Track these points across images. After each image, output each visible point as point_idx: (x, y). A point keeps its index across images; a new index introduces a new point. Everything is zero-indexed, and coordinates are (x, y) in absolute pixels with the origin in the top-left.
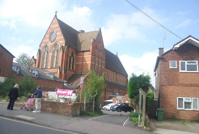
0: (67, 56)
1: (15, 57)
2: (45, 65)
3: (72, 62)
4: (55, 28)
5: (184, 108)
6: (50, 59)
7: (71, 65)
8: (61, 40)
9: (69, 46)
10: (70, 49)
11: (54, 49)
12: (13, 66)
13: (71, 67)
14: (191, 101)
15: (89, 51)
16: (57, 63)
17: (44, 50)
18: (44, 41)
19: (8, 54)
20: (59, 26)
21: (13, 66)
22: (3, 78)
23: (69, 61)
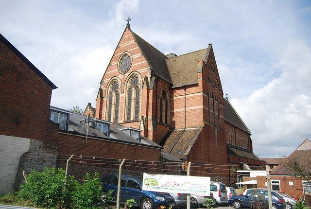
0: (155, 95)
1: (55, 87)
2: (112, 117)
3: (164, 108)
4: (130, 46)
5: (279, 184)
6: (122, 106)
7: (164, 114)
8: (142, 67)
9: (159, 78)
10: (160, 84)
11: (128, 85)
12: (52, 112)
13: (164, 118)
14: (126, 186)
15: (197, 85)
16: (137, 112)
17: (109, 89)
18: (109, 72)
19: (39, 78)
20: (136, 43)
21: (52, 112)
22: (28, 140)
23: (159, 105)
